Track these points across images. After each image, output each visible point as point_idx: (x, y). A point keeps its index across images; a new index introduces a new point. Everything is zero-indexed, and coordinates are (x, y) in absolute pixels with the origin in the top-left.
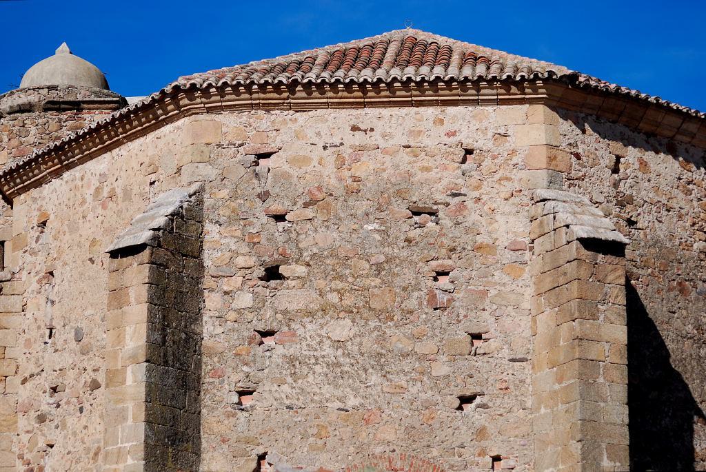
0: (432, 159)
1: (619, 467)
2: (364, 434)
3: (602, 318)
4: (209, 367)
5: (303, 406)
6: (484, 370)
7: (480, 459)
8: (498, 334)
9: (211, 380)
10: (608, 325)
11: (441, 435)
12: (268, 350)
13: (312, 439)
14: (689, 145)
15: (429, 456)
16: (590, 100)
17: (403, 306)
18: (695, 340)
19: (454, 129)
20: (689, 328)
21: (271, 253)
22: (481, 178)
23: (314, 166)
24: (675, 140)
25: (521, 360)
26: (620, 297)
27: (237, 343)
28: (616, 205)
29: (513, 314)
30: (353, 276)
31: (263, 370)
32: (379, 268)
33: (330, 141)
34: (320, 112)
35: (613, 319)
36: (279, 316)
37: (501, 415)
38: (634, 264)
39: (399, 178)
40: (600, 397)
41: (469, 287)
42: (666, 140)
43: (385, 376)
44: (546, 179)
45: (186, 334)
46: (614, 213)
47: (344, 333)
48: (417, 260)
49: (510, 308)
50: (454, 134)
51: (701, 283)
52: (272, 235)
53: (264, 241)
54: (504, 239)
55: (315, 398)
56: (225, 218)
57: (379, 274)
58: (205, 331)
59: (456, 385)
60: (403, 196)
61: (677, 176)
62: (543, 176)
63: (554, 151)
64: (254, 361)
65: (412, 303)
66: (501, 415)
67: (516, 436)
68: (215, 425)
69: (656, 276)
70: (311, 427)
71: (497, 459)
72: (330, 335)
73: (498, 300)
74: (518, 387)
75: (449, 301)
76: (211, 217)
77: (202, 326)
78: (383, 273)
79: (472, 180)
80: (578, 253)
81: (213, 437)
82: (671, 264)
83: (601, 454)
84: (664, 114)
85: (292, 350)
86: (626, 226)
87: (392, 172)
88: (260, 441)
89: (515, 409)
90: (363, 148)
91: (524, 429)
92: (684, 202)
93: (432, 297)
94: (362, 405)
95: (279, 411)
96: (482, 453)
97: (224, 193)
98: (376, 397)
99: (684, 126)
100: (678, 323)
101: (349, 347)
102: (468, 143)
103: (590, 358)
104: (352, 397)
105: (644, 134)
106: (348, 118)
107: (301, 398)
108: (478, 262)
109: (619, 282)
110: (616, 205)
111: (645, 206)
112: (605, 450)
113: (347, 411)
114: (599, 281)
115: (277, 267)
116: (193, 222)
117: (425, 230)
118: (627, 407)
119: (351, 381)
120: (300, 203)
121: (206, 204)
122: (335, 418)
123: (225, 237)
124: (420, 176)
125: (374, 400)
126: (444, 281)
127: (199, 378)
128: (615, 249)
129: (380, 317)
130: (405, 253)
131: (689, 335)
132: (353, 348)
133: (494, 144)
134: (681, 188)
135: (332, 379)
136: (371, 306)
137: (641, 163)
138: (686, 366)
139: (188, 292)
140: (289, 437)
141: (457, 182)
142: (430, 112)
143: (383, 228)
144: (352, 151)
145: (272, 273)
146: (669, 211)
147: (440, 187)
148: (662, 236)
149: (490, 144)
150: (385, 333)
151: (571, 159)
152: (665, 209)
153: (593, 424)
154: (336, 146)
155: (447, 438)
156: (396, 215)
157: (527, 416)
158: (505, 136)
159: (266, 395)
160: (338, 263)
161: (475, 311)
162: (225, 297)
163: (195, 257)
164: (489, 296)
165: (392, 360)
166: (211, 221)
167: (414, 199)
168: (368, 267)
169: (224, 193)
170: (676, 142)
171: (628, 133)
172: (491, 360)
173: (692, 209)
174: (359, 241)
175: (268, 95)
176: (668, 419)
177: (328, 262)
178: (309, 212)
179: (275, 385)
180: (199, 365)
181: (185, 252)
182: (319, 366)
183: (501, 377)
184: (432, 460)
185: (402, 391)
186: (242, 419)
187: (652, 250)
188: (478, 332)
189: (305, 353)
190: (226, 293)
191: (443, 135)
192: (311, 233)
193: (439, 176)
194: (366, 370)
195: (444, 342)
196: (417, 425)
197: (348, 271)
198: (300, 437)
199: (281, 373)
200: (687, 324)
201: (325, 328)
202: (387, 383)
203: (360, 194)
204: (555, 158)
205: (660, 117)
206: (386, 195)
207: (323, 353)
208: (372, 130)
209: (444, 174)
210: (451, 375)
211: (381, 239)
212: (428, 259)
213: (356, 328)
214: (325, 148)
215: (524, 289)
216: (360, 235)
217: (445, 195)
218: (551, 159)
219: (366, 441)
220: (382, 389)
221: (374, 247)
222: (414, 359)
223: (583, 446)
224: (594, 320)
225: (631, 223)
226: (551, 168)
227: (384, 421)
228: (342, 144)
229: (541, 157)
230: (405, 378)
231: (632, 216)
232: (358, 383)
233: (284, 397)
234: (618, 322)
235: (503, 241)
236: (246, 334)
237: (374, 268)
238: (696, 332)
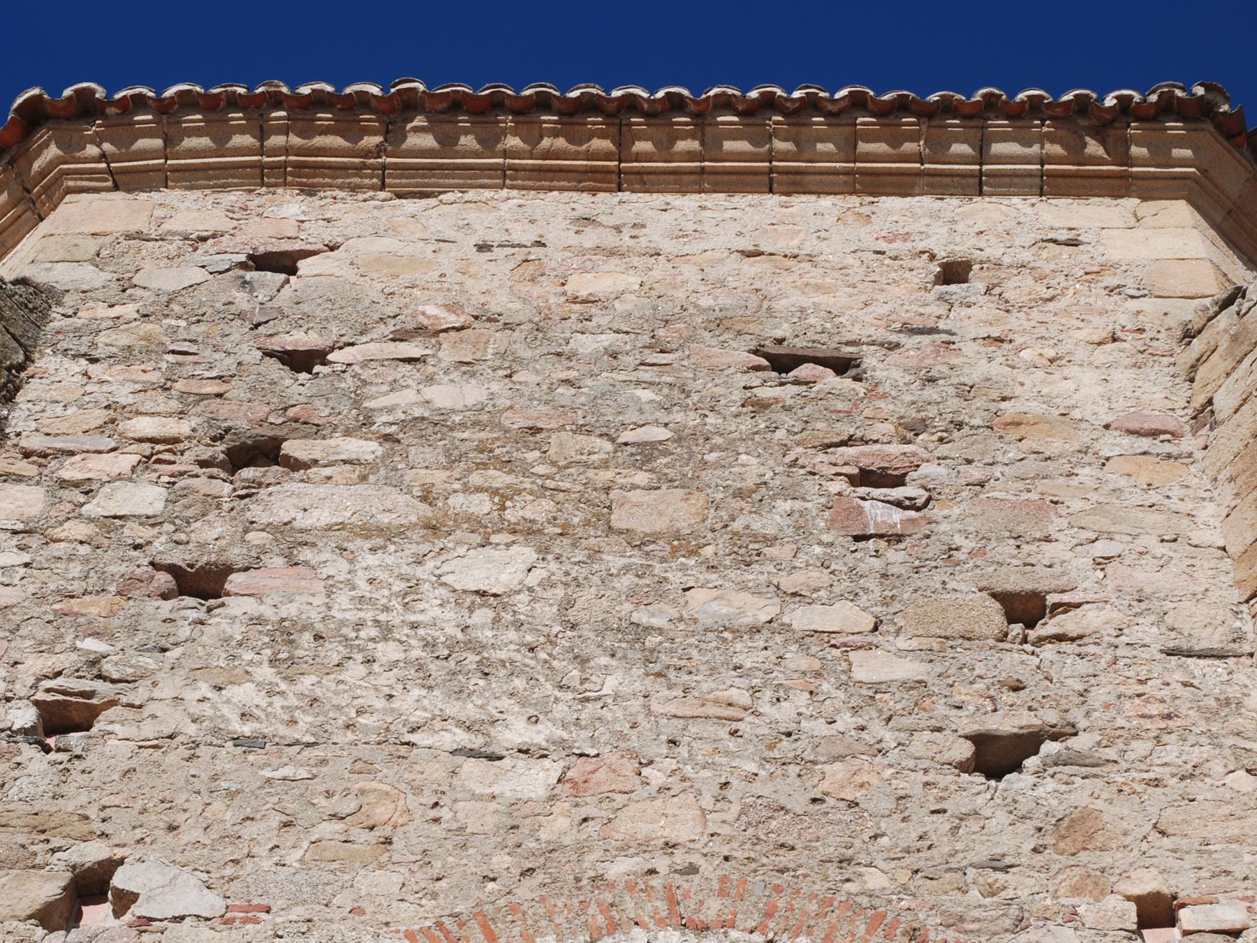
31: (164, 650)
66: (1157, 783)
175: (319, 141)
232: (549, 688)
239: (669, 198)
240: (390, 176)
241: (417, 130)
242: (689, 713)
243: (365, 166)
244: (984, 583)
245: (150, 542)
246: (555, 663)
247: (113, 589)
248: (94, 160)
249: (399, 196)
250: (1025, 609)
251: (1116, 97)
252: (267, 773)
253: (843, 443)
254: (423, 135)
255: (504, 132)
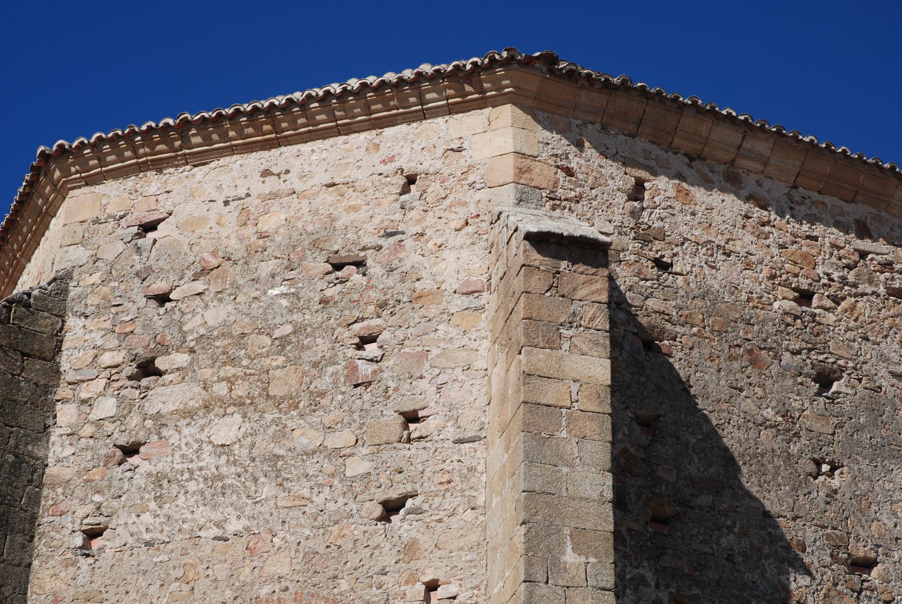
0: (361, 195)
1: (594, 564)
2: (248, 570)
3: (566, 346)
4: (50, 502)
5: (167, 540)
6: (419, 461)
7: (407, 589)
8: (439, 409)
9: (51, 519)
10: (575, 357)
11: (353, 560)
12: (130, 470)
13: (175, 585)
14: (762, 176)
15: (336, 591)
16: (586, 97)
17: (312, 387)
18: (779, 430)
19: (392, 154)
20: (769, 413)
21: (147, 343)
22: (425, 208)
23: (211, 228)
24: (739, 168)
25: (472, 440)
26: (599, 319)
27: (91, 464)
28: (635, 239)
29: (462, 377)
30: (249, 357)
31: (120, 497)
32: (283, 342)
33: (232, 193)
34: (224, 161)
35: (585, 349)
36: (149, 423)
37: (440, 521)
38: (667, 317)
39: (318, 225)
40: (561, 457)
41: (402, 351)
42: (723, 167)
43: (281, 485)
44: (512, 195)
45: (16, 456)
46: (630, 248)
47: (231, 434)
48: (335, 326)
49: (458, 371)
50: (392, 159)
51: (788, 354)
52: (150, 320)
53: (138, 330)
54: (453, 281)
55: (185, 526)
56: (93, 308)
57: (282, 350)
58: (51, 455)
59: (378, 484)
60: (320, 246)
61: (743, 213)
62: (509, 194)
63: (528, 162)
64: (110, 486)
65: (324, 383)
66: (440, 521)
67: (461, 549)
68: (48, 580)
69: (706, 338)
70: (175, 568)
71: (432, 586)
72: (212, 438)
73: (442, 362)
74: (465, 477)
75: (374, 372)
76: (75, 309)
77: (47, 448)
78: (289, 348)
79: (413, 212)
80: (527, 257)
81: (43, 597)
82: (732, 324)
83: (561, 544)
84: (710, 125)
85: (162, 466)
86: (653, 268)
87: (310, 218)
88: (105, 596)
89: (460, 510)
90: (274, 196)
91: (473, 537)
92: (754, 246)
93: (353, 369)
94: (247, 529)
95: (135, 551)
96: (412, 579)
97: (96, 278)
98: (267, 516)
99: (747, 145)
100: (749, 405)
101: (236, 452)
102: (410, 167)
103: (544, 401)
104: (234, 519)
105: (686, 155)
106: (258, 162)
107: (166, 528)
108: (416, 316)
109: (598, 299)
110: (635, 239)
111: (686, 245)
112: (568, 538)
113: (226, 540)
114: (563, 296)
115: (153, 360)
116: (46, 314)
117: (349, 284)
118: (610, 476)
119: (234, 497)
120: (189, 274)
121: (71, 294)
122: (209, 551)
123: (91, 331)
124: (345, 219)
125: (265, 519)
126: (371, 350)
127: (33, 518)
128: (590, 252)
129: (281, 407)
130: (319, 317)
131: (768, 423)
132: (242, 453)
133: (444, 163)
134: (749, 228)
135: (209, 497)
136: (270, 393)
137: (678, 191)
138: (762, 465)
139: (26, 402)
140: (144, 585)
141: (393, 218)
142: (362, 138)
143: (293, 290)
144: (260, 201)
145: (147, 369)
146: (729, 256)
147: (370, 228)
148: (717, 286)
149: (439, 164)
150: (285, 426)
151: (556, 173)
152: (721, 251)
153: (548, 498)
154: (240, 199)
155: (362, 563)
156: (312, 272)
157: (477, 518)
158: (460, 150)
159: (120, 530)
160: (230, 344)
161: (409, 381)
162: (82, 407)
163: (44, 359)
164: (430, 357)
165: (293, 462)
166: (75, 314)
167: (336, 248)
168: (269, 342)
169: (96, 278)
170: (740, 171)
171: (656, 151)
172: (429, 445)
173: (769, 258)
174: (261, 311)
176: (732, 536)
177: (217, 344)
178: (199, 286)
179: (133, 515)
180: (35, 500)
181: (27, 351)
182: (194, 481)
183: (441, 466)
184: (338, 597)
185: (303, 502)
186: (85, 568)
187: (699, 302)
188: (412, 408)
189: (177, 467)
190: (84, 402)
191: (377, 162)
192: (200, 310)
193: (370, 214)
194: (255, 480)
195: (365, 428)
196: (322, 550)
197: (243, 352)
198: (159, 583)
199: (142, 498)
200: (764, 406)
201: (206, 430)
202: (283, 495)
203: (266, 253)
204: (529, 170)
205: (705, 127)
206: (299, 249)
207: (200, 464)
208: (287, 172)
209: (377, 211)
210: (373, 472)
211: (288, 304)
212: (349, 322)
213: (247, 425)
214: (226, 203)
215: (477, 343)
216: (262, 304)
217: (376, 236)
218: (521, 171)
219: (248, 580)
220: (276, 504)
221: (278, 317)
222: (322, 456)
223: (528, 531)
224: (551, 348)
225: (662, 265)
226: (522, 181)
227: (276, 549)
228: (248, 195)
229: (507, 169)
230: (308, 485)
231: (664, 256)
233: (144, 530)
234: (595, 354)
235: (452, 284)
236: (103, 452)
237: (277, 342)
238: (780, 419)
239: (299, 146)
241: (194, 135)
242: (290, 505)
243: (178, 156)
244: (396, 408)
246: (247, 483)
247: (102, 464)
249: (195, 166)
250: (411, 417)
251: (471, 63)
252: (155, 560)
253: (356, 322)
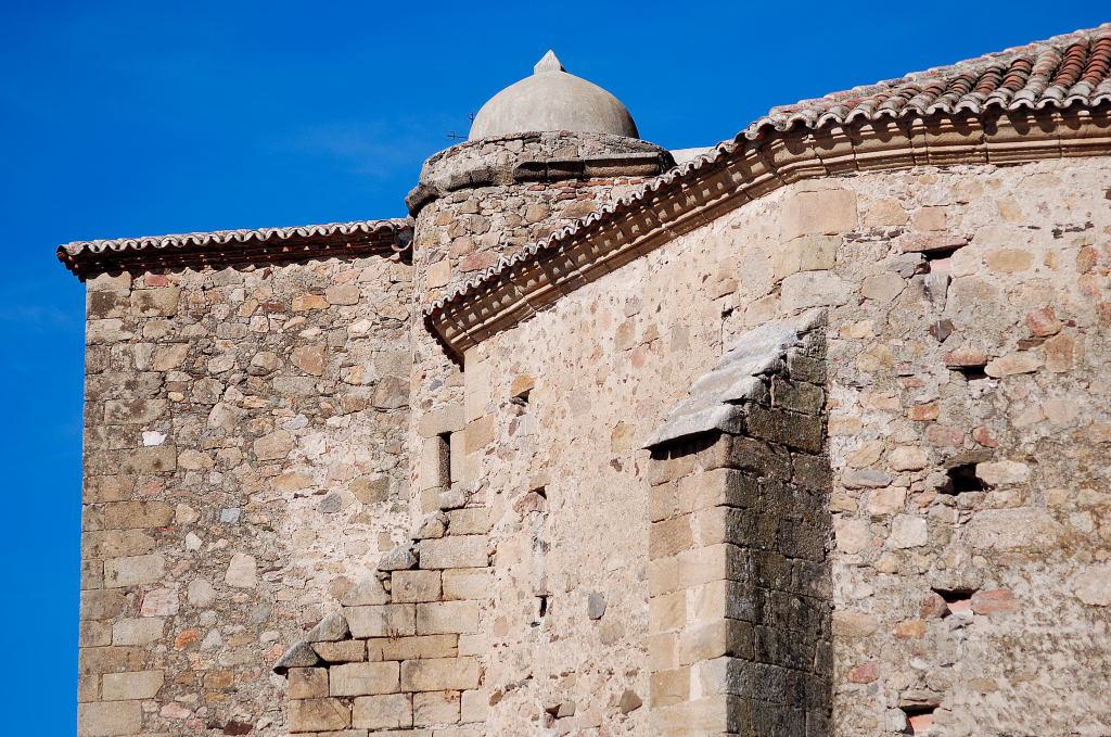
175: (944, 137)
240: (991, 155)
245: (927, 571)
248: (812, 158)
254: (1007, 129)
255: (1057, 124)
